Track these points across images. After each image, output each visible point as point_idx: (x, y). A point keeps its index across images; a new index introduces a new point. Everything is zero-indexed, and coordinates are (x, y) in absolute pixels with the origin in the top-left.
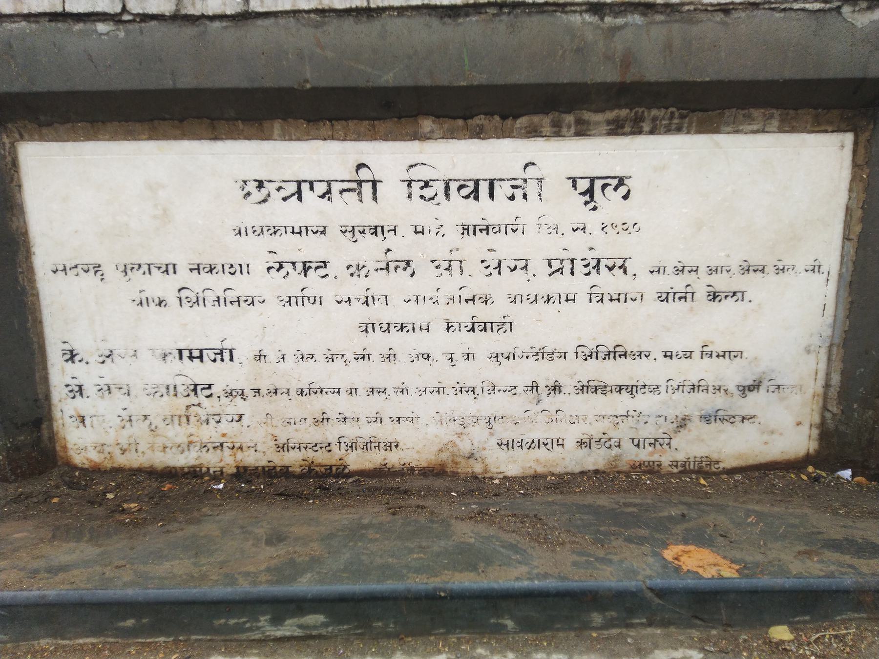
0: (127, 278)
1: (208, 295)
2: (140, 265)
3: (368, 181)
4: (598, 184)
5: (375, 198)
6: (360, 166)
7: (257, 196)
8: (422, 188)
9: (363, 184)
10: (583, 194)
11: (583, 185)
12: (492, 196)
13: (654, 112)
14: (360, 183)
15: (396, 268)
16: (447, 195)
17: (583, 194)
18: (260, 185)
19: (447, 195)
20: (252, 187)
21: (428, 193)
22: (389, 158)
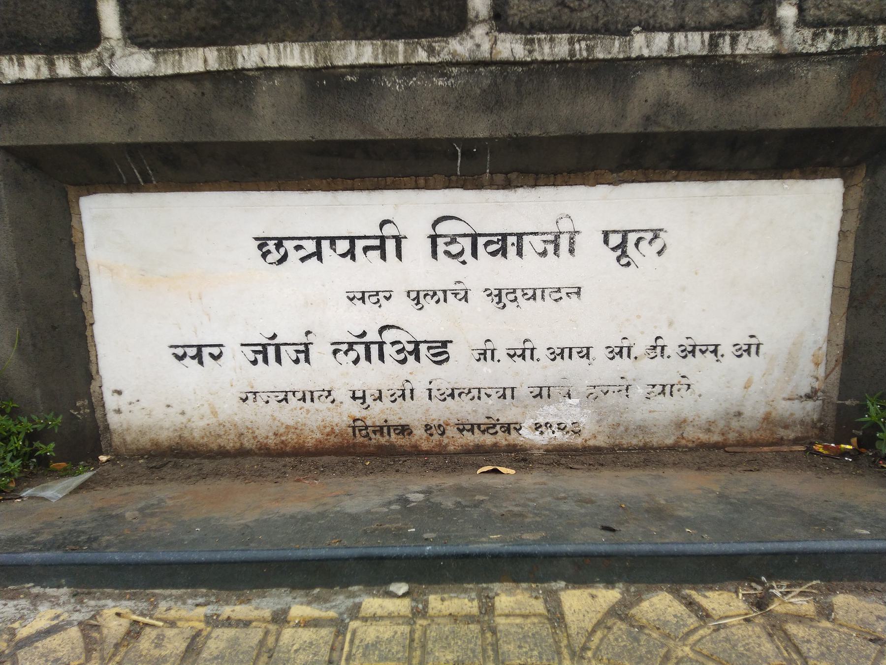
0: (419, 306)
1: (687, 293)
2: (435, 294)
3: (465, 235)
4: (632, 238)
5: (399, 255)
6: (383, 223)
7: (275, 256)
8: (446, 244)
9: (356, 241)
10: (413, 300)
11: (615, 240)
12: (520, 253)
13: (560, 36)
14: (383, 239)
15: (460, 395)
16: (474, 254)
17: (413, 300)
18: (279, 245)
19: (474, 254)
20: (271, 245)
21: (454, 249)
22: (411, 210)
